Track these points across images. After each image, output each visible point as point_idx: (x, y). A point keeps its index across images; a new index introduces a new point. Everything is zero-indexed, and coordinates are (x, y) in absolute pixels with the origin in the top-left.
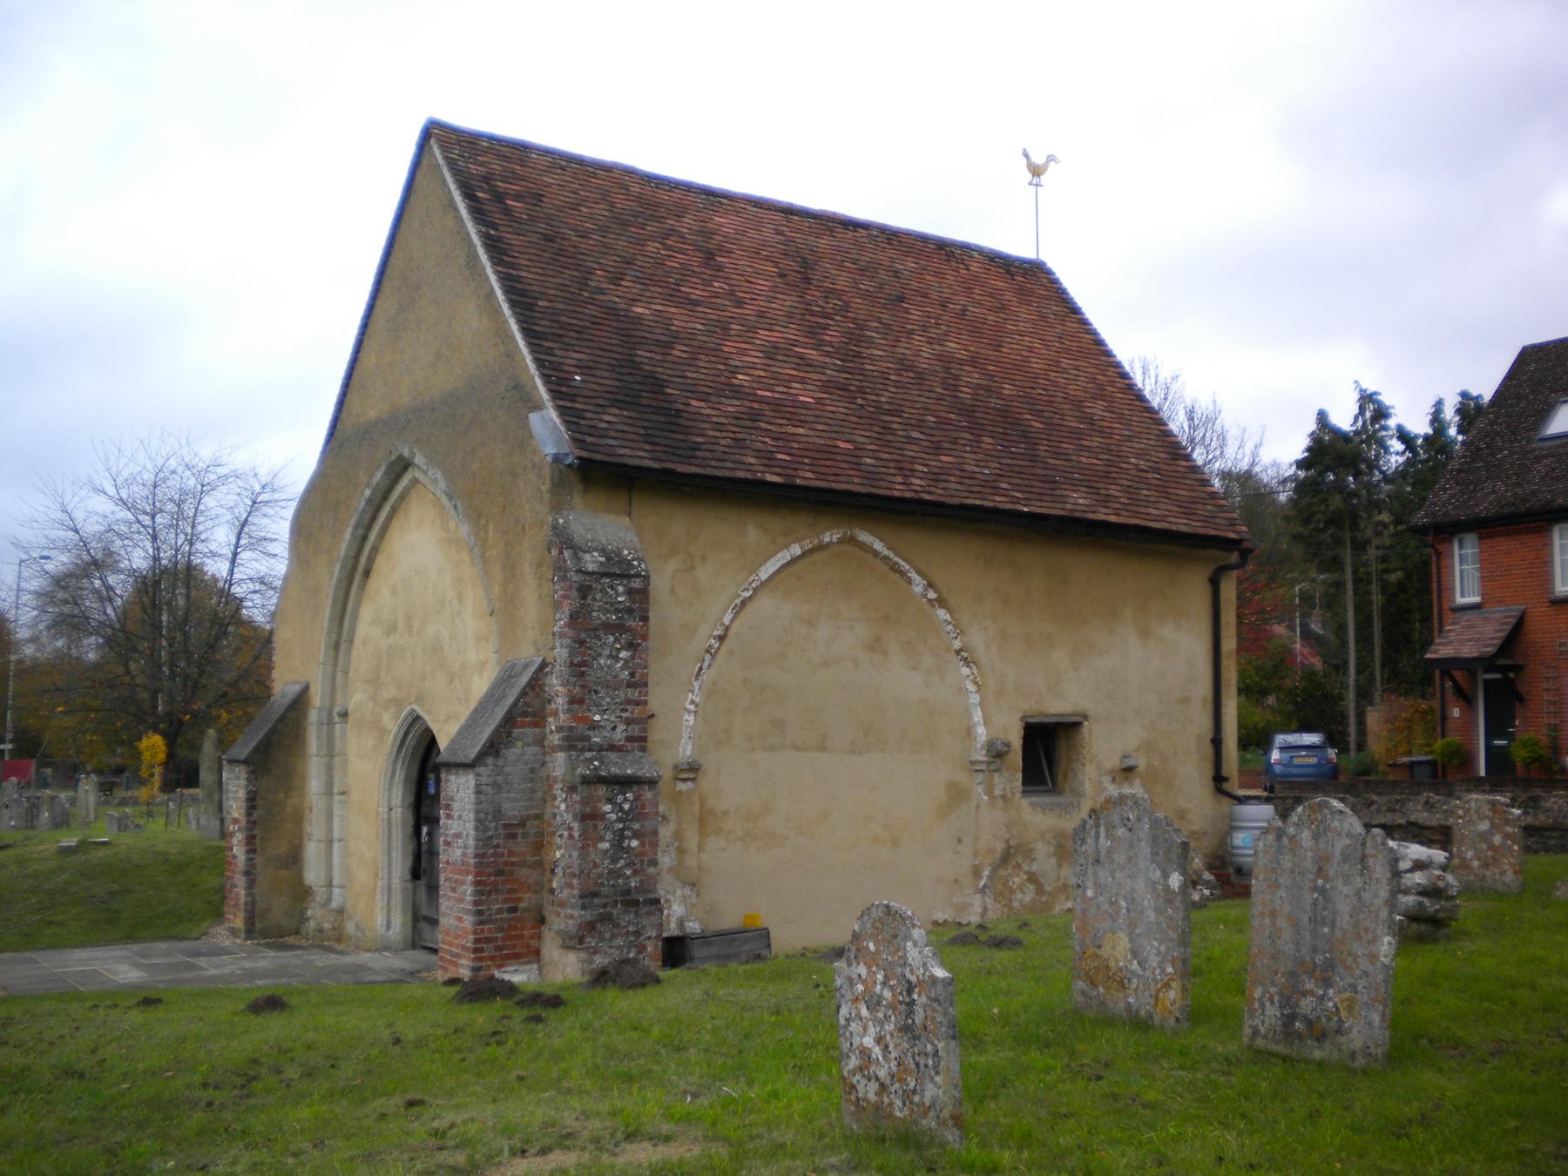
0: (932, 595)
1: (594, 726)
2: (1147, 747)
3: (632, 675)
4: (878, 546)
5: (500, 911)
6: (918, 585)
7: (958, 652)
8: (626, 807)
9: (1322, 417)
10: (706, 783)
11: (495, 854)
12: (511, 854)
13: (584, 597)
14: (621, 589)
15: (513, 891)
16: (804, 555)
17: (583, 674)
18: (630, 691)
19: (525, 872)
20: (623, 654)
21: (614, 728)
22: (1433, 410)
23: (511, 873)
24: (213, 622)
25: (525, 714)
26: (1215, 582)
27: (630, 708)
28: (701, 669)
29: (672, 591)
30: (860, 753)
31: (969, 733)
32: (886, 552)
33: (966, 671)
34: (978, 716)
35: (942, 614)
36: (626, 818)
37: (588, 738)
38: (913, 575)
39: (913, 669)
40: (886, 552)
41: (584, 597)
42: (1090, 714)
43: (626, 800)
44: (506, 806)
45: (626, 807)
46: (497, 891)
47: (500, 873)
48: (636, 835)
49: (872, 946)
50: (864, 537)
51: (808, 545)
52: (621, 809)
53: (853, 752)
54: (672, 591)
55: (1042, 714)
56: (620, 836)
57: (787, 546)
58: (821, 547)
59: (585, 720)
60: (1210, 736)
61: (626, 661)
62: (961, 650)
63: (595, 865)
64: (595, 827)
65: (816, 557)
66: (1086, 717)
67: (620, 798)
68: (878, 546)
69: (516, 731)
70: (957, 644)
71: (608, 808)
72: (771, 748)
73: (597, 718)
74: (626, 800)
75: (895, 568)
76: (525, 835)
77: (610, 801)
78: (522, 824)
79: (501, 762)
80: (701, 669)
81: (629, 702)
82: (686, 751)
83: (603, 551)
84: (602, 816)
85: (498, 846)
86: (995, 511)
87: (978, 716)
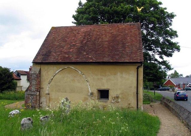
2: (122, 94)
4: (73, 68)
6: (80, 72)
7: (87, 80)
9: (178, 43)
10: (50, 95)
16: (62, 70)
26: (138, 69)
29: (45, 75)
34: (90, 89)
36: (32, 98)
38: (79, 71)
48: (33, 100)
49: (121, 117)
50: (71, 67)
51: (62, 69)
54: (45, 75)
55: (100, 89)
56: (31, 101)
57: (60, 69)
68: (73, 68)
70: (86, 80)
72: (58, 92)
75: (76, 70)
82: (47, 92)
84: (30, 98)
86: (83, 62)
87: (90, 89)
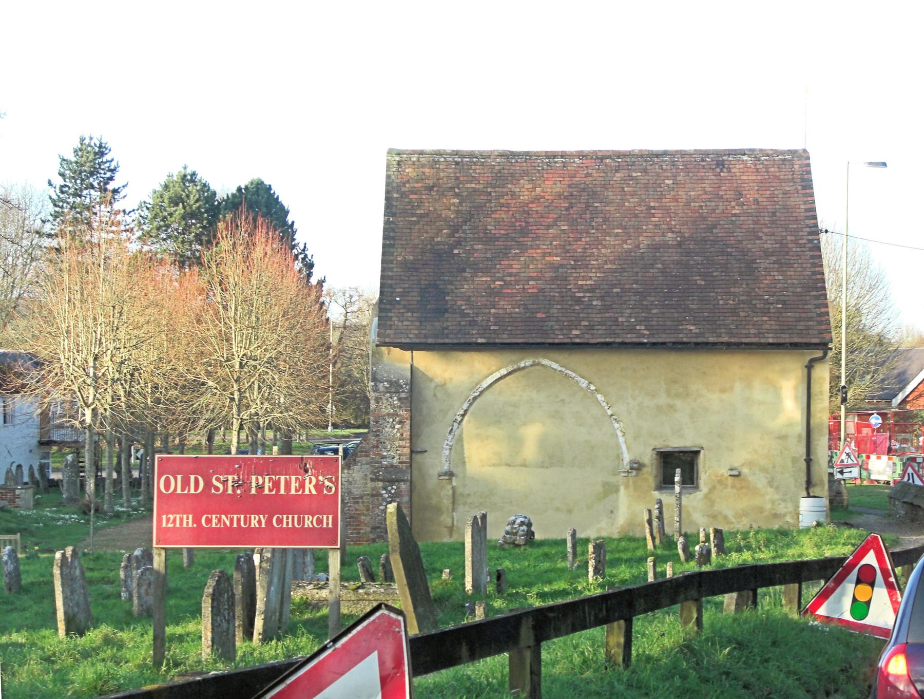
0: (593, 387)
1: (384, 457)
3: (402, 435)
4: (555, 366)
5: (352, 533)
8: (393, 491)
11: (348, 510)
12: (356, 510)
13: (378, 403)
14: (395, 398)
15: (358, 525)
16: (509, 374)
17: (378, 435)
18: (401, 442)
19: (363, 518)
20: (397, 426)
21: (393, 458)
22: (290, 219)
23: (357, 518)
24: (899, 375)
25: (362, 452)
26: (809, 367)
27: (401, 449)
28: (452, 429)
30: (547, 468)
31: (619, 457)
32: (560, 369)
33: (616, 425)
35: (600, 397)
37: (381, 462)
39: (580, 425)
40: (560, 369)
41: (378, 403)
42: (704, 446)
43: (392, 488)
44: (354, 490)
45: (393, 491)
46: (350, 525)
47: (352, 517)
50: (545, 362)
52: (390, 493)
53: (542, 467)
58: (519, 369)
59: (379, 455)
60: (805, 457)
61: (398, 429)
62: (612, 415)
63: (378, 516)
64: (378, 500)
65: (517, 374)
66: (702, 448)
67: (389, 488)
69: (358, 459)
71: (384, 492)
73: (385, 454)
74: (392, 488)
76: (363, 502)
77: (385, 489)
78: (361, 497)
79: (351, 472)
80: (452, 429)
81: (400, 447)
83: (390, 382)
85: (350, 506)
